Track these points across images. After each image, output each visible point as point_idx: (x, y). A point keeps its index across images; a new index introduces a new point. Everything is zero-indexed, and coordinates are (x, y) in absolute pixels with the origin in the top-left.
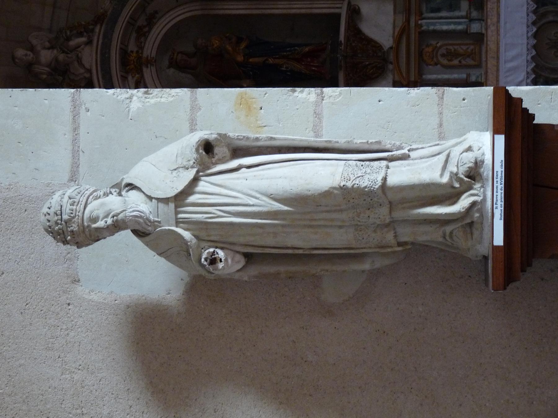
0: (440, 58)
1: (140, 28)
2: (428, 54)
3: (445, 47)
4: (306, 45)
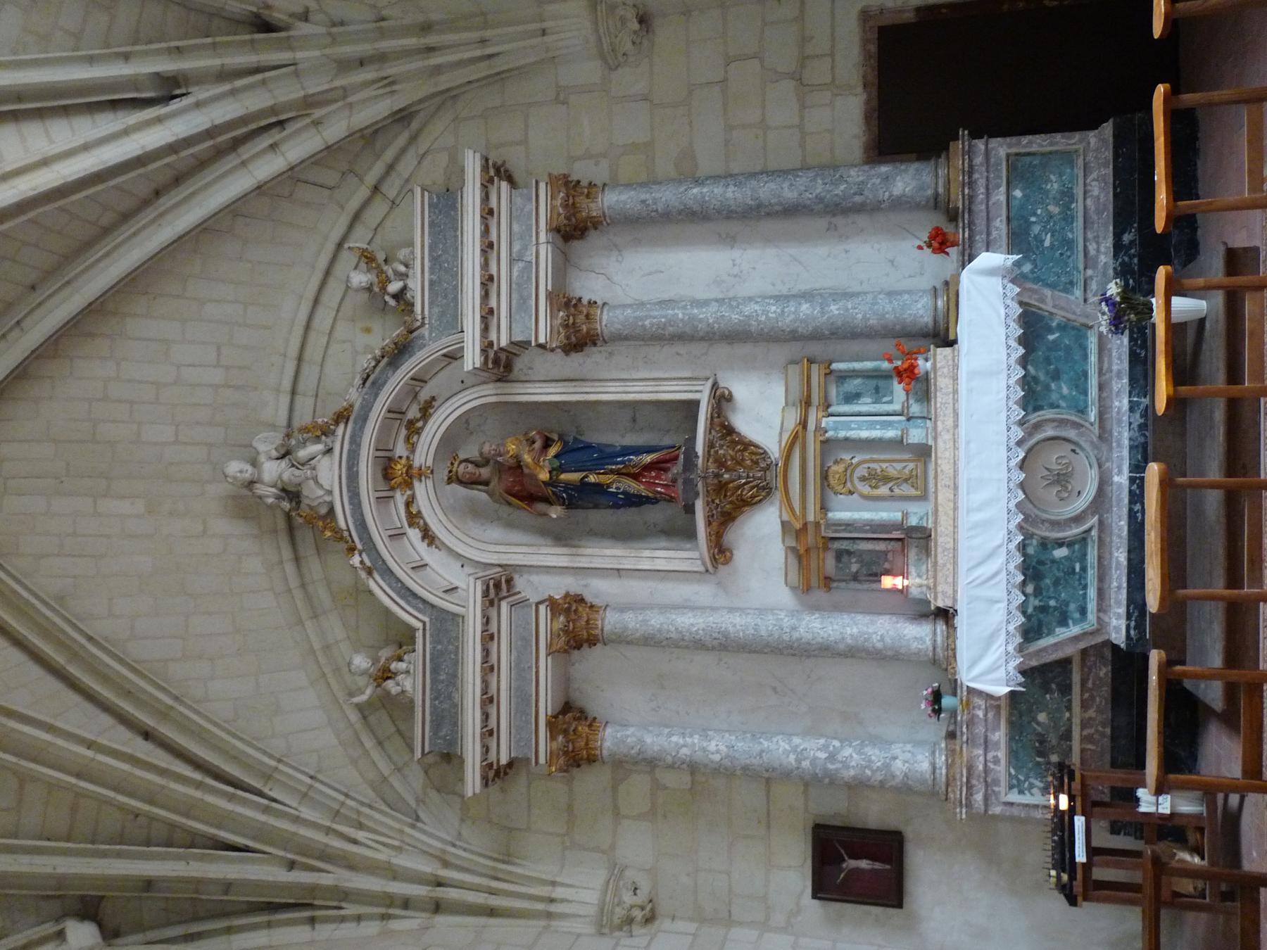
0: (856, 481)
1: (411, 423)
2: (837, 476)
3: (866, 465)
4: (649, 450)
